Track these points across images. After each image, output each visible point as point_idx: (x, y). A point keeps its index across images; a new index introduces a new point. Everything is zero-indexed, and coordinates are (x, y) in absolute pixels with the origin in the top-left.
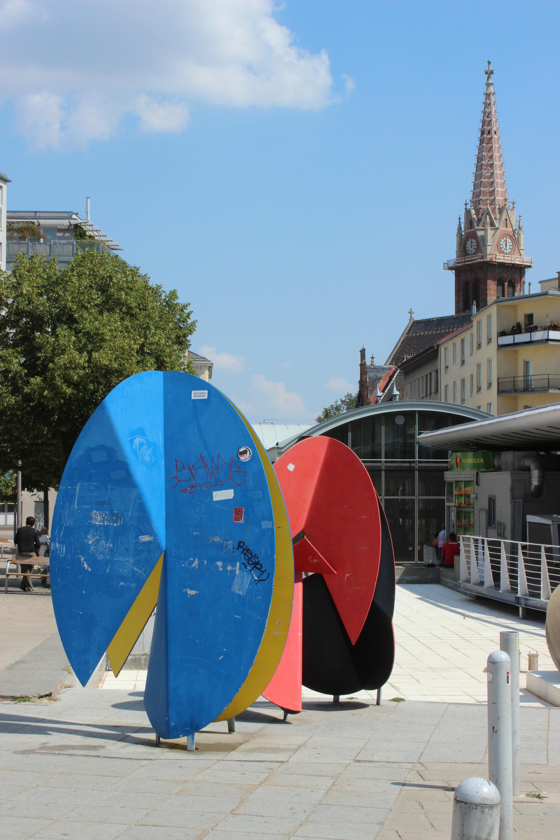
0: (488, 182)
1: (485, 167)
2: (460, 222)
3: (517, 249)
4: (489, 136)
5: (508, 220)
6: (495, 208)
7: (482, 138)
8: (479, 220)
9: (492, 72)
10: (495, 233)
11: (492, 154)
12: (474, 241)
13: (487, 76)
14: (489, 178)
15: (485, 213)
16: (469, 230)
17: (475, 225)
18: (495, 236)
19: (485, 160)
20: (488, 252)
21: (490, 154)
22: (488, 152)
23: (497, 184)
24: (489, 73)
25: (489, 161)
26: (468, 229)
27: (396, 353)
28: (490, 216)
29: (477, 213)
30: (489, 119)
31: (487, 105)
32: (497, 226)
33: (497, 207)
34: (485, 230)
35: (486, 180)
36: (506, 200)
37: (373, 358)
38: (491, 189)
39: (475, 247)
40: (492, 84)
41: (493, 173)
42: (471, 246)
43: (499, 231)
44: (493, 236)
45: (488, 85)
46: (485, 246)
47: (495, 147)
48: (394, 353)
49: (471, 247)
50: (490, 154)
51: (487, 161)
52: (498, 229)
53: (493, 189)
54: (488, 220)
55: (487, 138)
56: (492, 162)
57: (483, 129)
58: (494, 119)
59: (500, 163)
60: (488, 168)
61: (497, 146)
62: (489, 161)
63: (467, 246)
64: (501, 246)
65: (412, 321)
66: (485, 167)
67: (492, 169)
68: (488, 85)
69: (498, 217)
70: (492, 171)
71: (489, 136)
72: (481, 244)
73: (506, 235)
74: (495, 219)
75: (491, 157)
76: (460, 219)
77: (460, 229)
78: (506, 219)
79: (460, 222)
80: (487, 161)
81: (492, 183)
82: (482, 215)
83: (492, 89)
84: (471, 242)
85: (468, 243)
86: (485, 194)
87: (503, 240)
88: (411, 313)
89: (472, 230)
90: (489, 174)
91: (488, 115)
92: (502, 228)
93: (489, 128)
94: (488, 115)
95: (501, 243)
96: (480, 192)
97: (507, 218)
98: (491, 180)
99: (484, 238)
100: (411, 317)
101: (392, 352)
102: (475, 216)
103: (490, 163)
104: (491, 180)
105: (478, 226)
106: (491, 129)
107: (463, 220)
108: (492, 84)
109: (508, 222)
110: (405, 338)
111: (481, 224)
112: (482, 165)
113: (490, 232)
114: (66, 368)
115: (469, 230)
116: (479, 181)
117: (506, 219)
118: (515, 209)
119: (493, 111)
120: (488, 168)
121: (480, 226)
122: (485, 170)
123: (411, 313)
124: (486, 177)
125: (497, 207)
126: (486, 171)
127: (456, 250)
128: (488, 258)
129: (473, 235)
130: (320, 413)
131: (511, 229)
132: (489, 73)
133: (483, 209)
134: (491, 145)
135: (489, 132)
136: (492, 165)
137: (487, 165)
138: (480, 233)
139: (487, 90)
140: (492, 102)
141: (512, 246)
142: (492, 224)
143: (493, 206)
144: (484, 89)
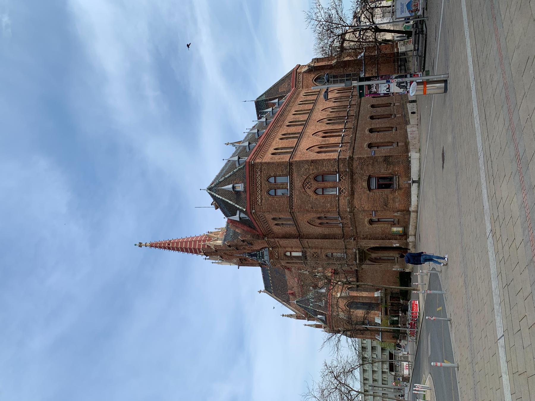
107: (214, 261)
123: (260, 292)
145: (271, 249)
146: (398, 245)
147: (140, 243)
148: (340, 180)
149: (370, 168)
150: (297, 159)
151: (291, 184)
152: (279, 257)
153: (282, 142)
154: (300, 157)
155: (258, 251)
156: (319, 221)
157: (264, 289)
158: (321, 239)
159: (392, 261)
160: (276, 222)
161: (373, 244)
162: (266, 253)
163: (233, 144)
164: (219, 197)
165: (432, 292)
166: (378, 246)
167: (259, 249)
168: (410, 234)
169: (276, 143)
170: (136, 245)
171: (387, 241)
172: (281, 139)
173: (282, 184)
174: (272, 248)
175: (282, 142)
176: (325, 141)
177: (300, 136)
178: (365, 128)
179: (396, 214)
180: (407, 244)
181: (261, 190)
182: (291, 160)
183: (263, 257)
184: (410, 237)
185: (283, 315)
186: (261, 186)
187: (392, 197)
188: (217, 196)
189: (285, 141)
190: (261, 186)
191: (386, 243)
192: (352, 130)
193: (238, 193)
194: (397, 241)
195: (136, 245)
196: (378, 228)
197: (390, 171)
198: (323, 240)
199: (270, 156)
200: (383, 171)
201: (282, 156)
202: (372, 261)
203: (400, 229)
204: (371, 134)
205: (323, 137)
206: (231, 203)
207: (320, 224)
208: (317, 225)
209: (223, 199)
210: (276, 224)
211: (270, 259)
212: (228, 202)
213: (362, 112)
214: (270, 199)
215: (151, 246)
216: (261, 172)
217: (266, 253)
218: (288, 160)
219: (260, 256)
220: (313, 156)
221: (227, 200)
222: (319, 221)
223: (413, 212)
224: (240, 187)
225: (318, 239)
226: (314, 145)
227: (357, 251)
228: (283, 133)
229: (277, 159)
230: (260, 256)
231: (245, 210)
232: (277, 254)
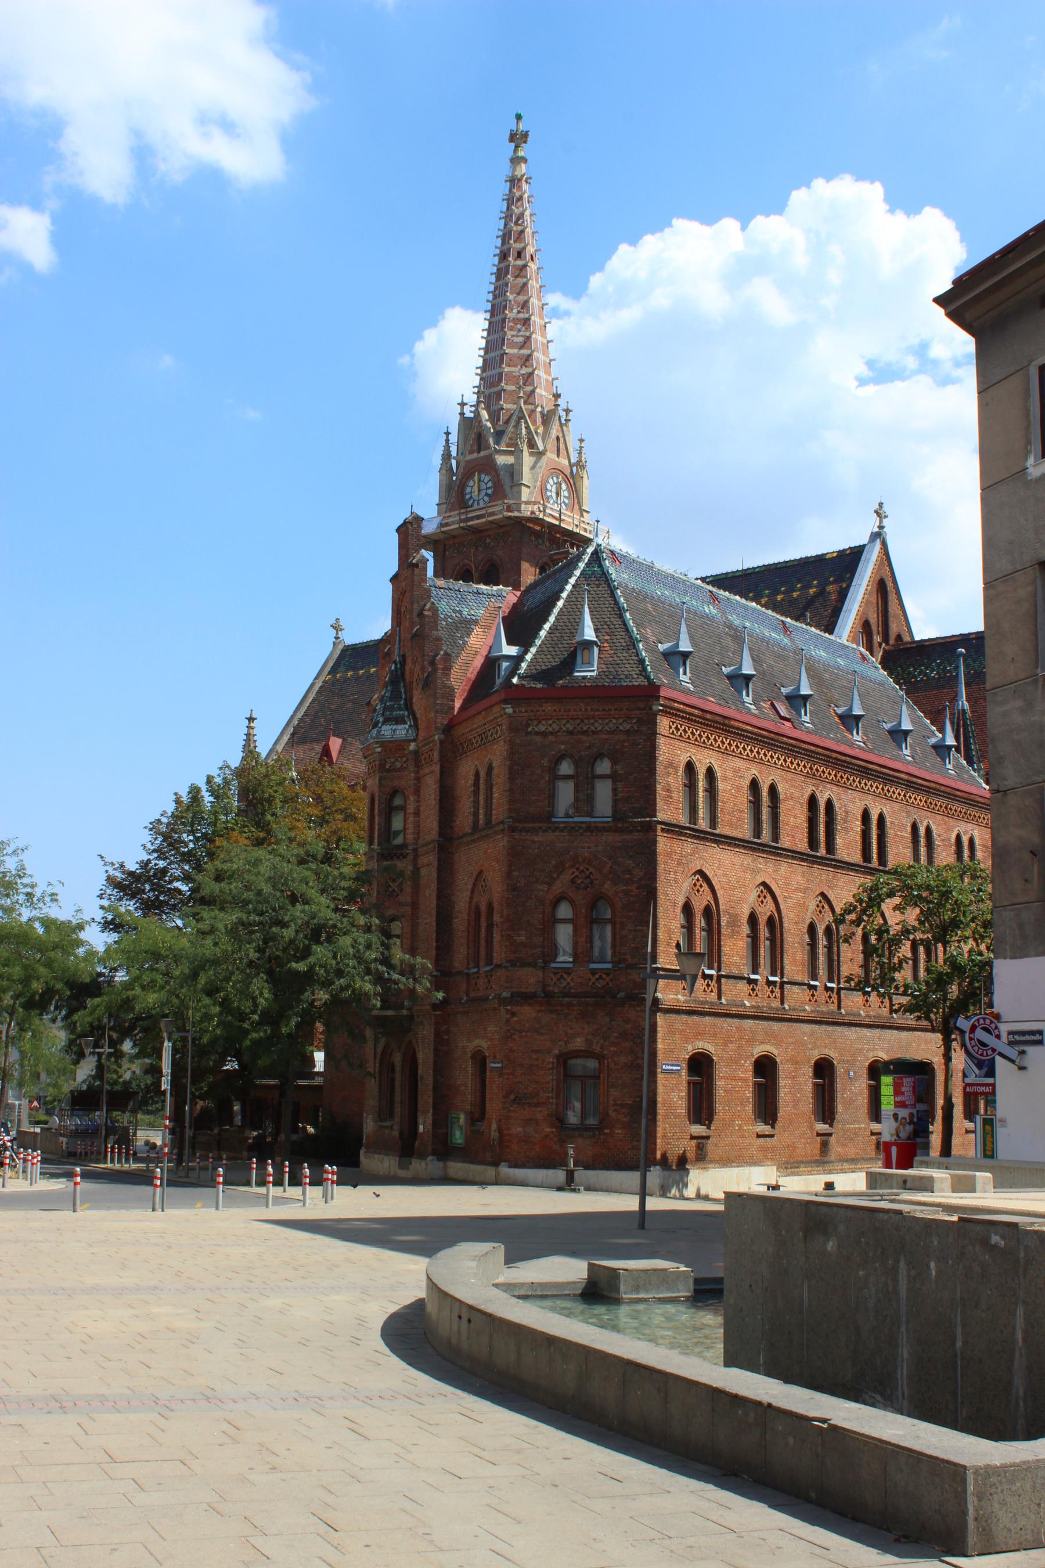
0: (519, 357)
1: (511, 324)
2: (447, 440)
3: (576, 507)
4: (519, 263)
5: (562, 440)
6: (533, 411)
7: (503, 265)
8: (499, 435)
9: (525, 136)
10: (536, 463)
11: (526, 298)
12: (487, 479)
13: (513, 145)
14: (521, 348)
15: (514, 417)
16: (475, 455)
17: (491, 440)
18: (537, 469)
19: (511, 310)
20: (524, 498)
21: (521, 298)
22: (518, 294)
23: (538, 363)
24: (518, 138)
25: (519, 312)
26: (471, 452)
27: (306, 714)
28: (526, 422)
29: (494, 418)
30: (520, 228)
31: (512, 200)
32: (541, 448)
33: (539, 409)
34: (517, 453)
35: (515, 351)
36: (557, 396)
37: (581, 440)
38: (524, 371)
39: (490, 492)
40: (524, 160)
41: (528, 338)
42: (477, 489)
43: (544, 459)
44: (533, 468)
45: (516, 161)
46: (517, 485)
47: (533, 287)
48: (300, 715)
49: (479, 491)
50: (521, 298)
51: (515, 311)
52: (542, 454)
53: (530, 370)
54: (524, 431)
55: (514, 266)
56: (527, 316)
57: (505, 248)
58: (529, 231)
59: (543, 323)
60: (519, 326)
61: (536, 286)
62: (519, 312)
63: (468, 490)
64: (549, 494)
65: (340, 647)
66: (511, 324)
67: (528, 328)
68: (516, 161)
69: (540, 430)
70: (528, 334)
71: (519, 263)
72: (505, 483)
73: (558, 471)
74: (536, 433)
75: (525, 305)
76: (448, 434)
77: (447, 456)
78: (558, 438)
79: (447, 440)
80: (515, 311)
81: (529, 357)
82: (507, 422)
83: (523, 168)
84: (479, 480)
85: (471, 483)
86: (512, 379)
87: (551, 481)
88: (337, 627)
89: (482, 454)
90: (521, 339)
91: (518, 219)
92: (551, 455)
93: (519, 246)
94: (518, 219)
95: (549, 487)
96: (500, 374)
97: (561, 435)
98: (525, 352)
99: (513, 472)
100: (337, 638)
101: (295, 712)
102: (489, 424)
103: (521, 316)
104: (525, 352)
105: (497, 443)
106: (524, 248)
107: (454, 438)
108: (524, 160)
109: (562, 446)
110: (325, 682)
111: (505, 439)
112: (504, 320)
113: (527, 460)
114: (307, 923)
115: (475, 455)
116: (498, 353)
117: (558, 438)
118: (570, 424)
119: (527, 213)
120: (519, 326)
121: (503, 444)
122: (511, 329)
123: (337, 627)
124: (513, 345)
125: (539, 409)
126: (514, 333)
127: (437, 500)
128: (526, 511)
129: (488, 466)
130: (950, 388)
131: (566, 462)
132: (518, 138)
133: (507, 410)
134: (525, 280)
135: (519, 255)
136: (526, 322)
137: (516, 321)
138: (501, 460)
139: (514, 170)
140: (526, 196)
141: (568, 498)
142: (532, 445)
143: (530, 407)
144: (506, 170)
145: (412, 746)
146: (421, 1128)
147: (525, 136)
148: (594, 972)
149: (623, 1059)
150: (663, 843)
151: (590, 828)
152: (388, 771)
153: (738, 788)
154: (669, 855)
155: (409, 706)
156: (483, 907)
157: (349, 641)
158: (438, 906)
159: (385, 1112)
160: (482, 774)
161: (425, 1056)
162: (401, 731)
163: (878, 536)
164: (569, 587)
165: (903, 1373)
166: (420, 1072)
167: (415, 708)
168: (450, 1164)
169: (735, 772)
170: (519, 117)
171: (431, 1101)
172: (754, 785)
173: (590, 800)
174: (416, 753)
175: (738, 788)
176: (734, 922)
177: (763, 844)
178: (777, 1045)
179: (494, 1126)
180: (422, 1156)
181: (570, 733)
182: (659, 827)
183: (387, 721)
184: (441, 1164)
185: (251, 719)
186: (585, 733)
187: (539, 1116)
188: (572, 581)
189: (744, 799)
190: (585, 733)
191: (426, 1098)
192: (776, 1004)
193: (569, 663)
194: (430, 1127)
195: (519, 117)
196: (464, 1076)
197: (613, 1114)
198: (434, 911)
199: (684, 759)
200: (615, 1093)
201: (679, 795)
202: (383, 1052)
203: (458, 1137)
204: (749, 1064)
205: (753, 919)
206: (543, 633)
207: (478, 908)
208: (475, 900)
209: (560, 604)
210: (477, 774)
211: (383, 744)
212: (546, 620)
213: (852, 1033)
214: (545, 762)
215: (514, 181)
216: (627, 732)
217: (401, 731)
218: (661, 816)
219: (391, 709)
220: (673, 889)
221: (552, 619)
222: (483, 907)
223: (498, 1174)
224: (588, 671)
225: (438, 898)
226: (720, 894)
227: (405, 1012)
228: (780, 788)
229: (669, 783)
230: (391, 709)
231: (515, 680)
232: (398, 765)
